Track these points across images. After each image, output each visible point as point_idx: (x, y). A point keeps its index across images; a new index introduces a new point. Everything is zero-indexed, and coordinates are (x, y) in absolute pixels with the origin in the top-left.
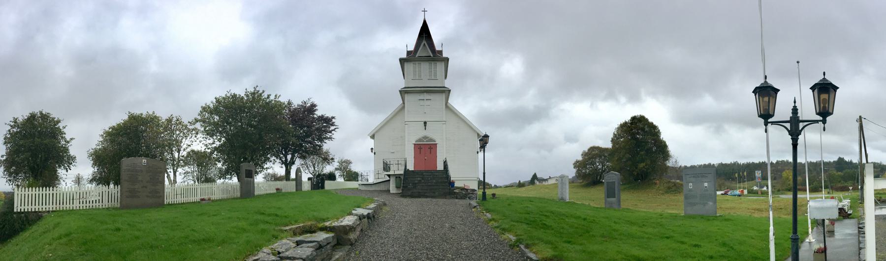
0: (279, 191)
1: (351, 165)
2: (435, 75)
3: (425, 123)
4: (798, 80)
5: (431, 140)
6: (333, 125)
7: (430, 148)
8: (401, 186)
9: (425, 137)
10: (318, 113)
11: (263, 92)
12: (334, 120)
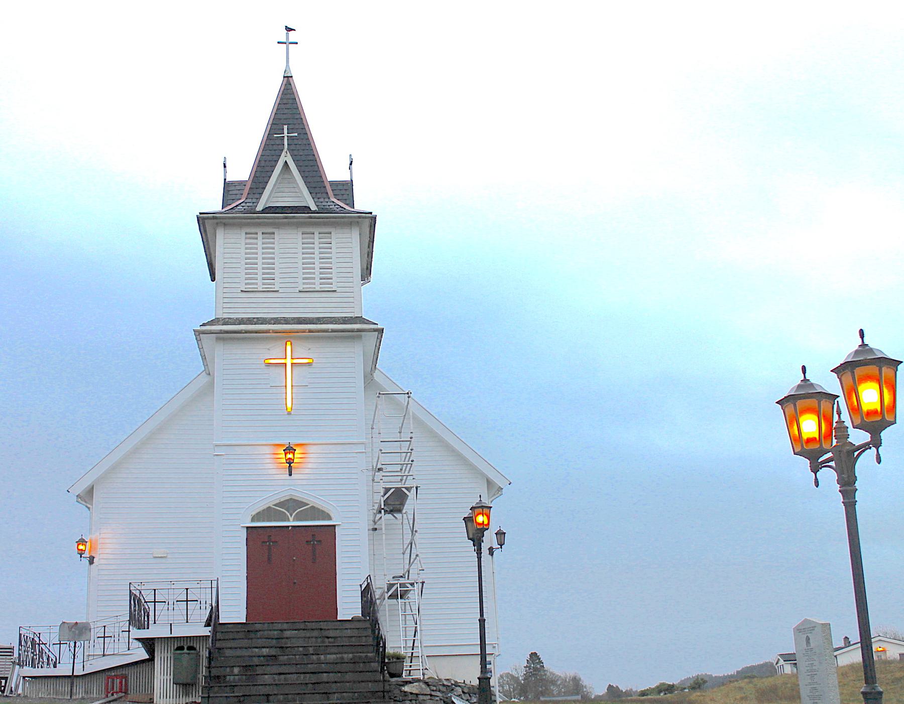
5: (317, 513)
8: (195, 677)
9: (291, 504)
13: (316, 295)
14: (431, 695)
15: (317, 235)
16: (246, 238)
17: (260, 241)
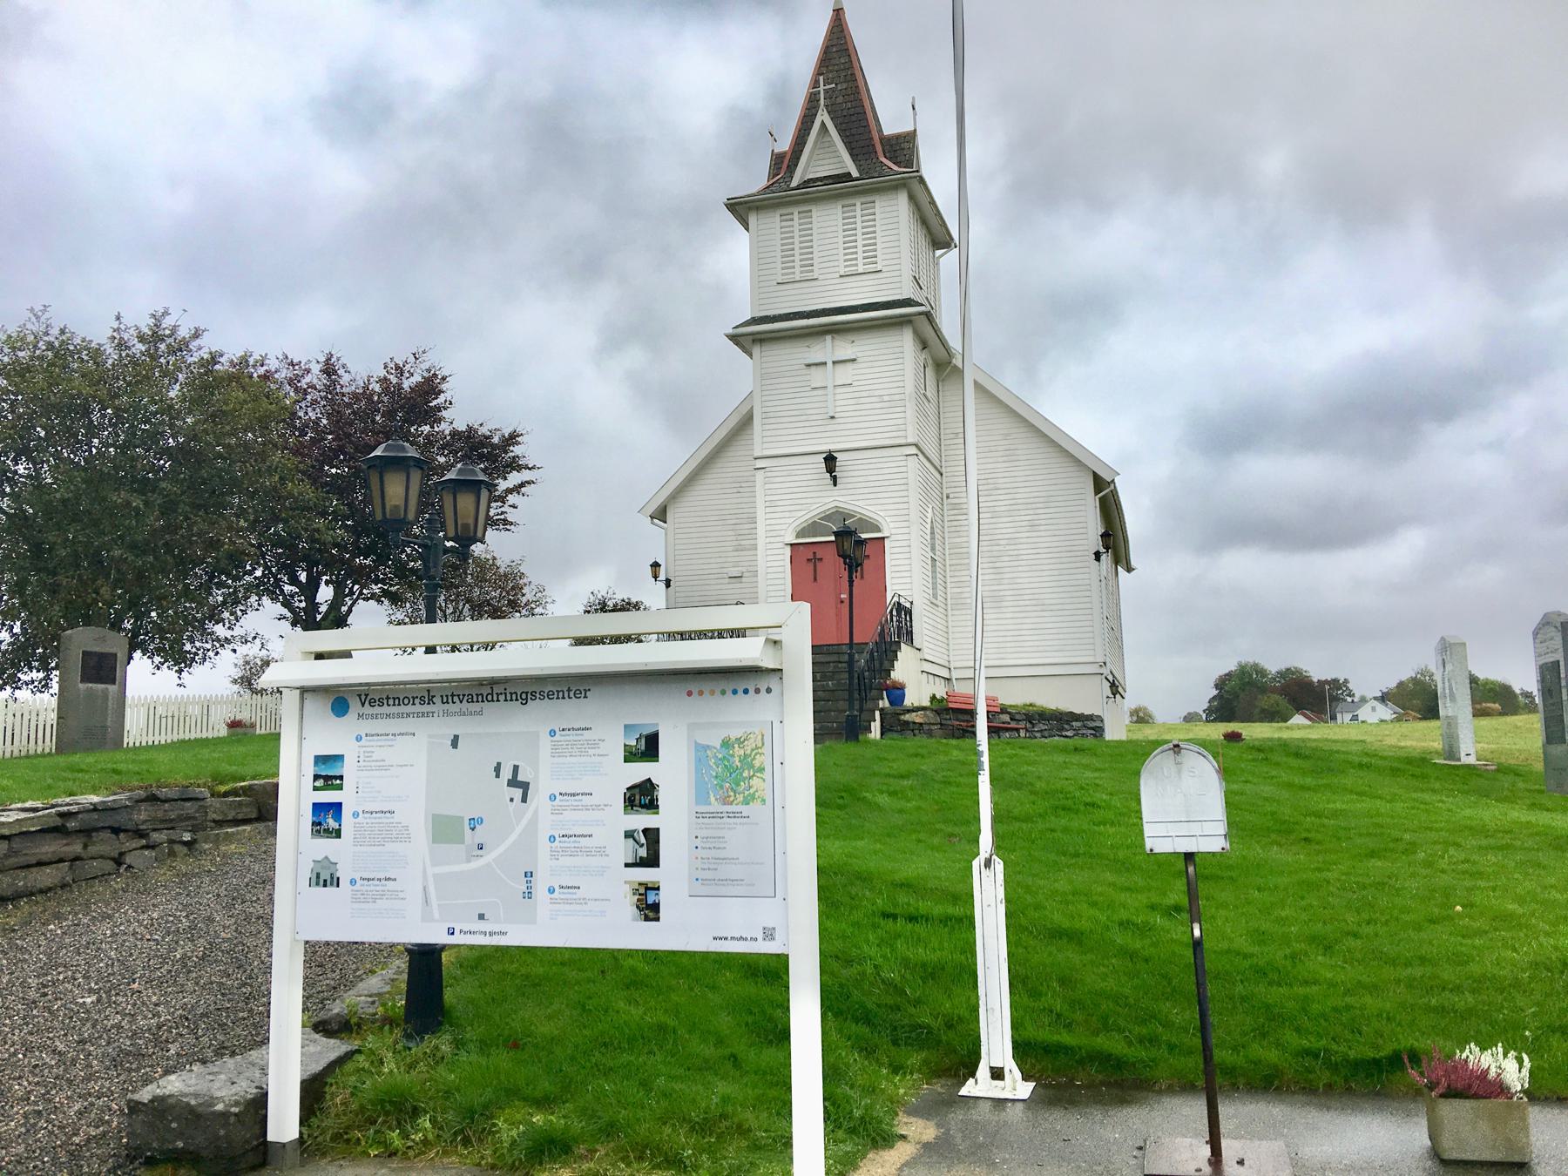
0: (239, 730)
2: (871, 258)
3: (830, 460)
4: (452, 501)
6: (515, 465)
10: (457, 418)
11: (196, 335)
12: (516, 450)
13: (858, 278)
14: (941, 724)
15: (858, 207)
16: (800, 219)
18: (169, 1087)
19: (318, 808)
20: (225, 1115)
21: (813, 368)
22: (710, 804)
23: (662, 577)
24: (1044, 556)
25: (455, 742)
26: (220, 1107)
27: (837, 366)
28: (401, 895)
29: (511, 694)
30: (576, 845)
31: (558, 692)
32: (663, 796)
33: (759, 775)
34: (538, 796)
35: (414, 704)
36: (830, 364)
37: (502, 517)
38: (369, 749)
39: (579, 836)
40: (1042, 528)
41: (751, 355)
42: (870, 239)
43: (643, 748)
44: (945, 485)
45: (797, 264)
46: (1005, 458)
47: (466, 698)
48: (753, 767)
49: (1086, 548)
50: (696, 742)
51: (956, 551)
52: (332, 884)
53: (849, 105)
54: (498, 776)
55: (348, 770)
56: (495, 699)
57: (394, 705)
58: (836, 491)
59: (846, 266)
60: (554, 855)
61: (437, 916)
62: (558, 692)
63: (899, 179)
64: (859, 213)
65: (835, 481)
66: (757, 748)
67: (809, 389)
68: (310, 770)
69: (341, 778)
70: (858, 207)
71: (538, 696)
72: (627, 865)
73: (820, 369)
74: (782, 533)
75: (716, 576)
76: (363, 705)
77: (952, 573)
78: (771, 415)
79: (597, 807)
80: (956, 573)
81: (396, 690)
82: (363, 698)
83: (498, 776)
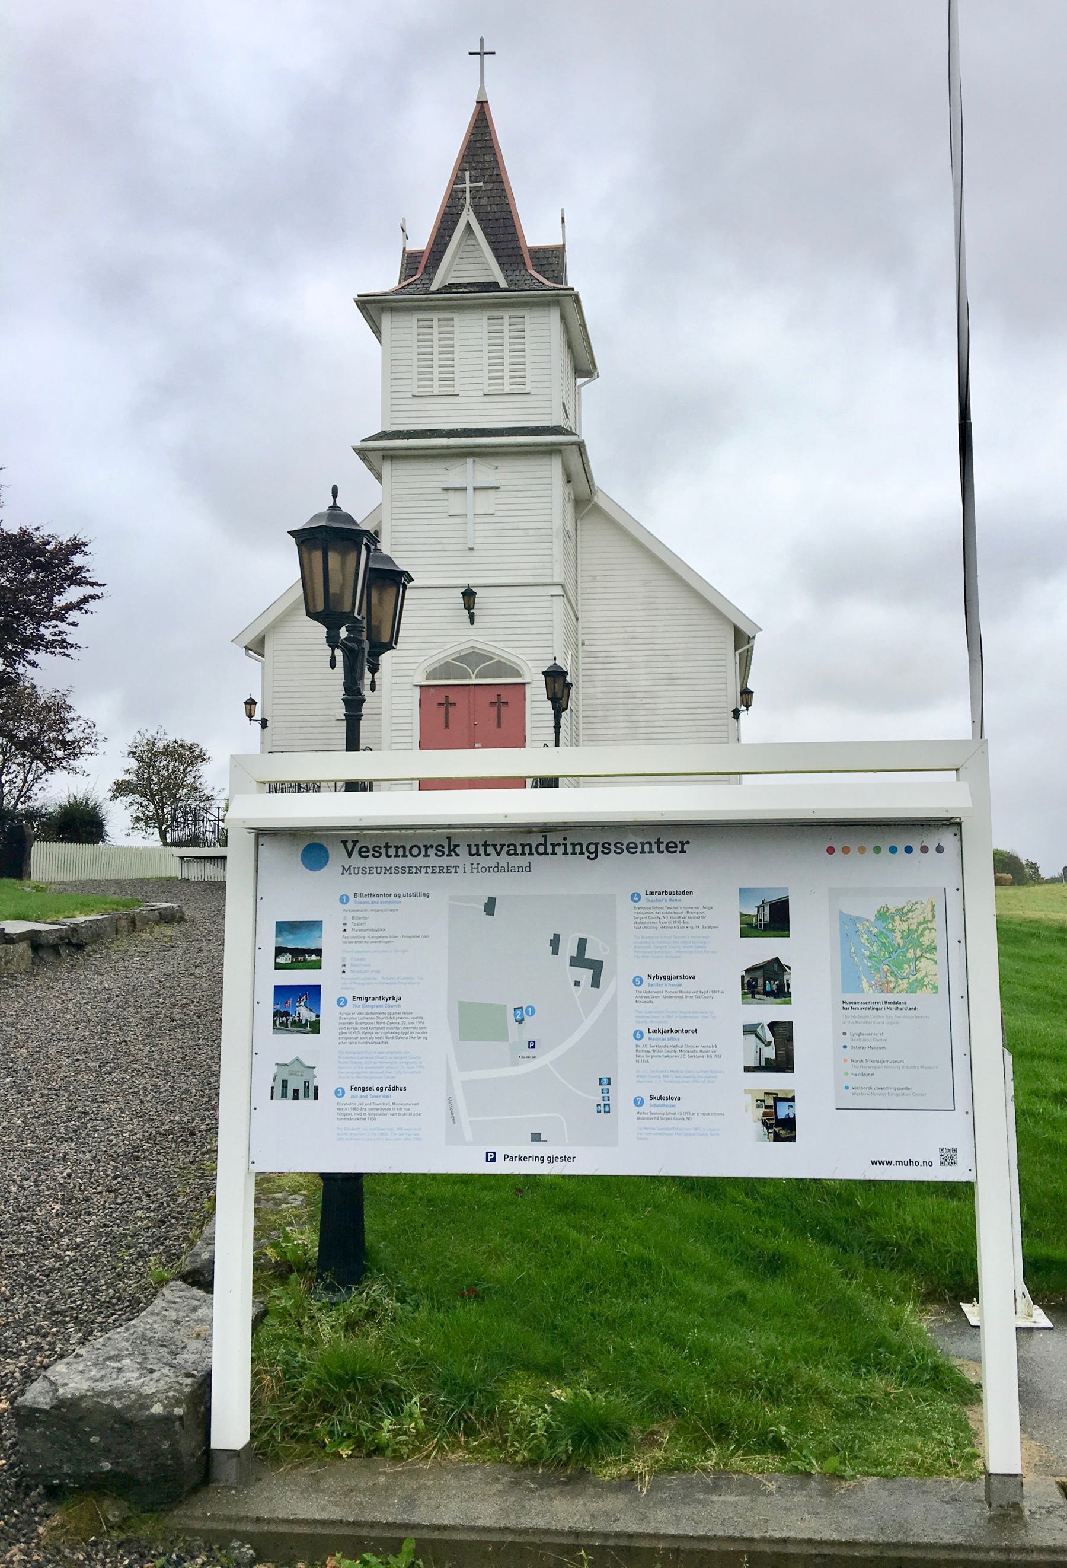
1: (203, 768)
2: (519, 377)
3: (469, 596)
5: (503, 668)
6: (76, 578)
7: (499, 704)
9: (474, 658)
12: (77, 560)
15: (506, 321)
16: (419, 327)
17: (435, 330)
18: (72, 1385)
19: (282, 992)
20: (167, 1420)
21: (451, 494)
22: (863, 991)
23: (258, 716)
24: (682, 711)
25: (490, 907)
26: (157, 1409)
27: (478, 492)
28: (414, 1109)
29: (573, 845)
30: (674, 1043)
31: (523, 846)
32: (795, 980)
33: (928, 955)
34: (616, 980)
35: (426, 855)
36: (470, 490)
37: (59, 638)
38: (360, 914)
39: (677, 1031)
40: (680, 682)
41: (379, 477)
42: (447, 359)
43: (767, 918)
44: (580, 631)
45: (436, 376)
46: (645, 606)
47: (505, 849)
48: (921, 945)
49: (724, 705)
50: (841, 912)
51: (591, 701)
52: (306, 1095)
53: (495, 208)
54: (555, 952)
55: (329, 942)
56: (550, 850)
57: (397, 856)
58: (472, 630)
59: (490, 385)
60: (642, 1057)
61: (468, 1135)
62: (643, 844)
63: (552, 295)
64: (506, 328)
65: (472, 617)
66: (925, 922)
67: (446, 515)
68: (269, 941)
69: (318, 952)
70: (506, 321)
71: (613, 848)
72: (747, 1069)
73: (459, 494)
74: (411, 673)
75: (322, 718)
76: (350, 855)
77: (585, 726)
78: (402, 541)
79: (703, 994)
80: (589, 726)
81: (399, 837)
82: (350, 846)
83: (555, 952)
